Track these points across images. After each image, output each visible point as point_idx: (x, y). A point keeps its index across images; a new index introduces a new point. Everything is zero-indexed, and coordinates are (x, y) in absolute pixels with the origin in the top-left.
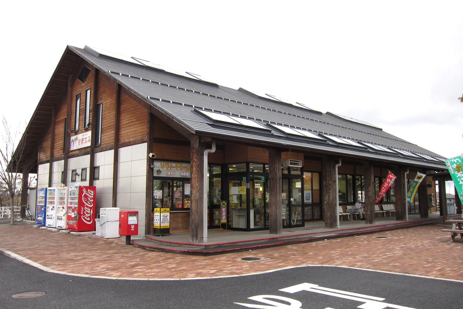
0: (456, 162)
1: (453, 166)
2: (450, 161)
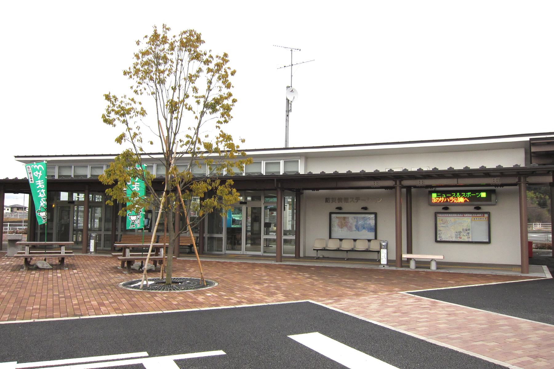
0: (38, 168)
1: (34, 173)
2: (32, 167)
